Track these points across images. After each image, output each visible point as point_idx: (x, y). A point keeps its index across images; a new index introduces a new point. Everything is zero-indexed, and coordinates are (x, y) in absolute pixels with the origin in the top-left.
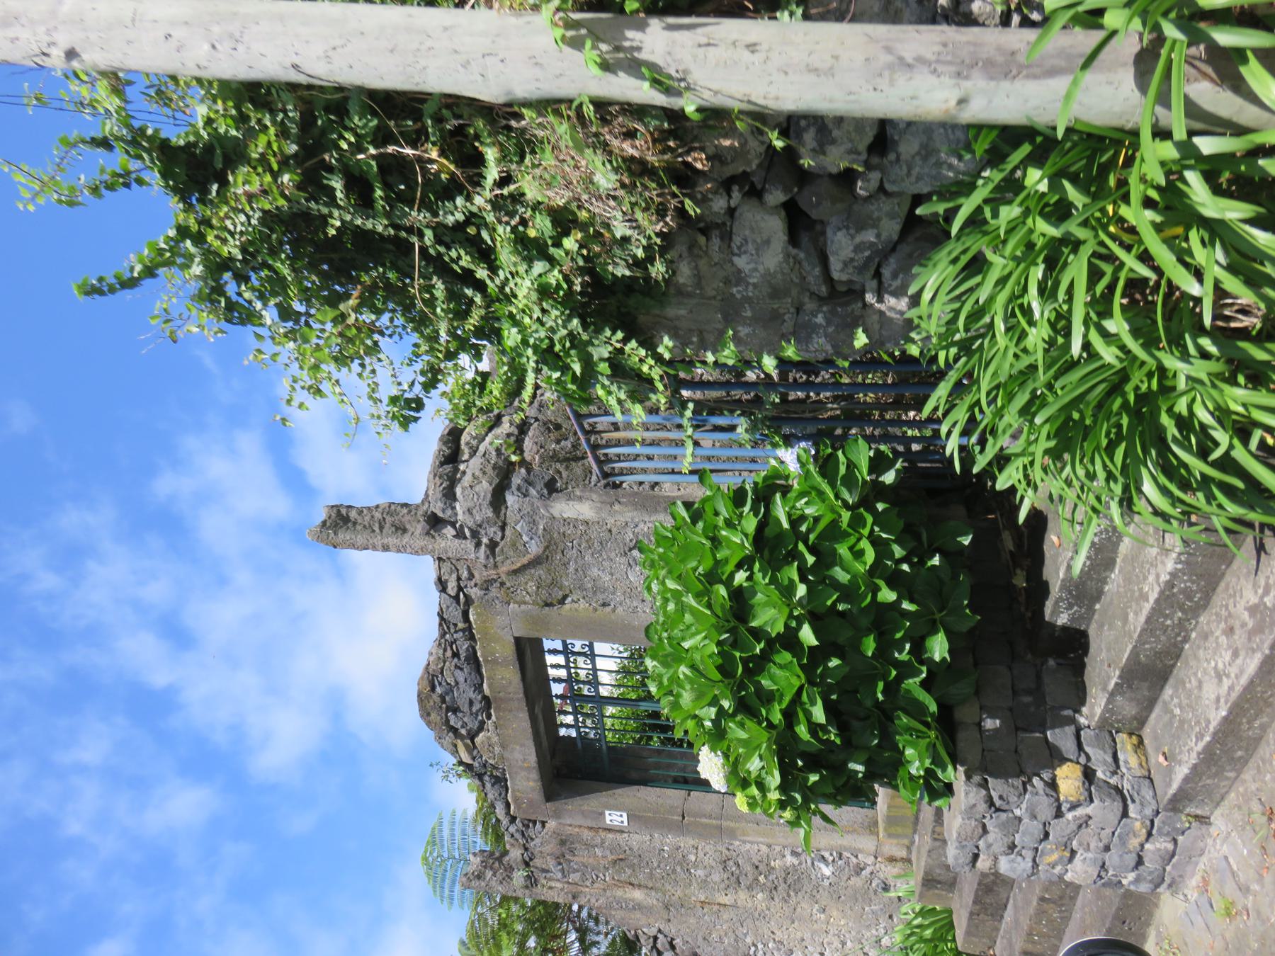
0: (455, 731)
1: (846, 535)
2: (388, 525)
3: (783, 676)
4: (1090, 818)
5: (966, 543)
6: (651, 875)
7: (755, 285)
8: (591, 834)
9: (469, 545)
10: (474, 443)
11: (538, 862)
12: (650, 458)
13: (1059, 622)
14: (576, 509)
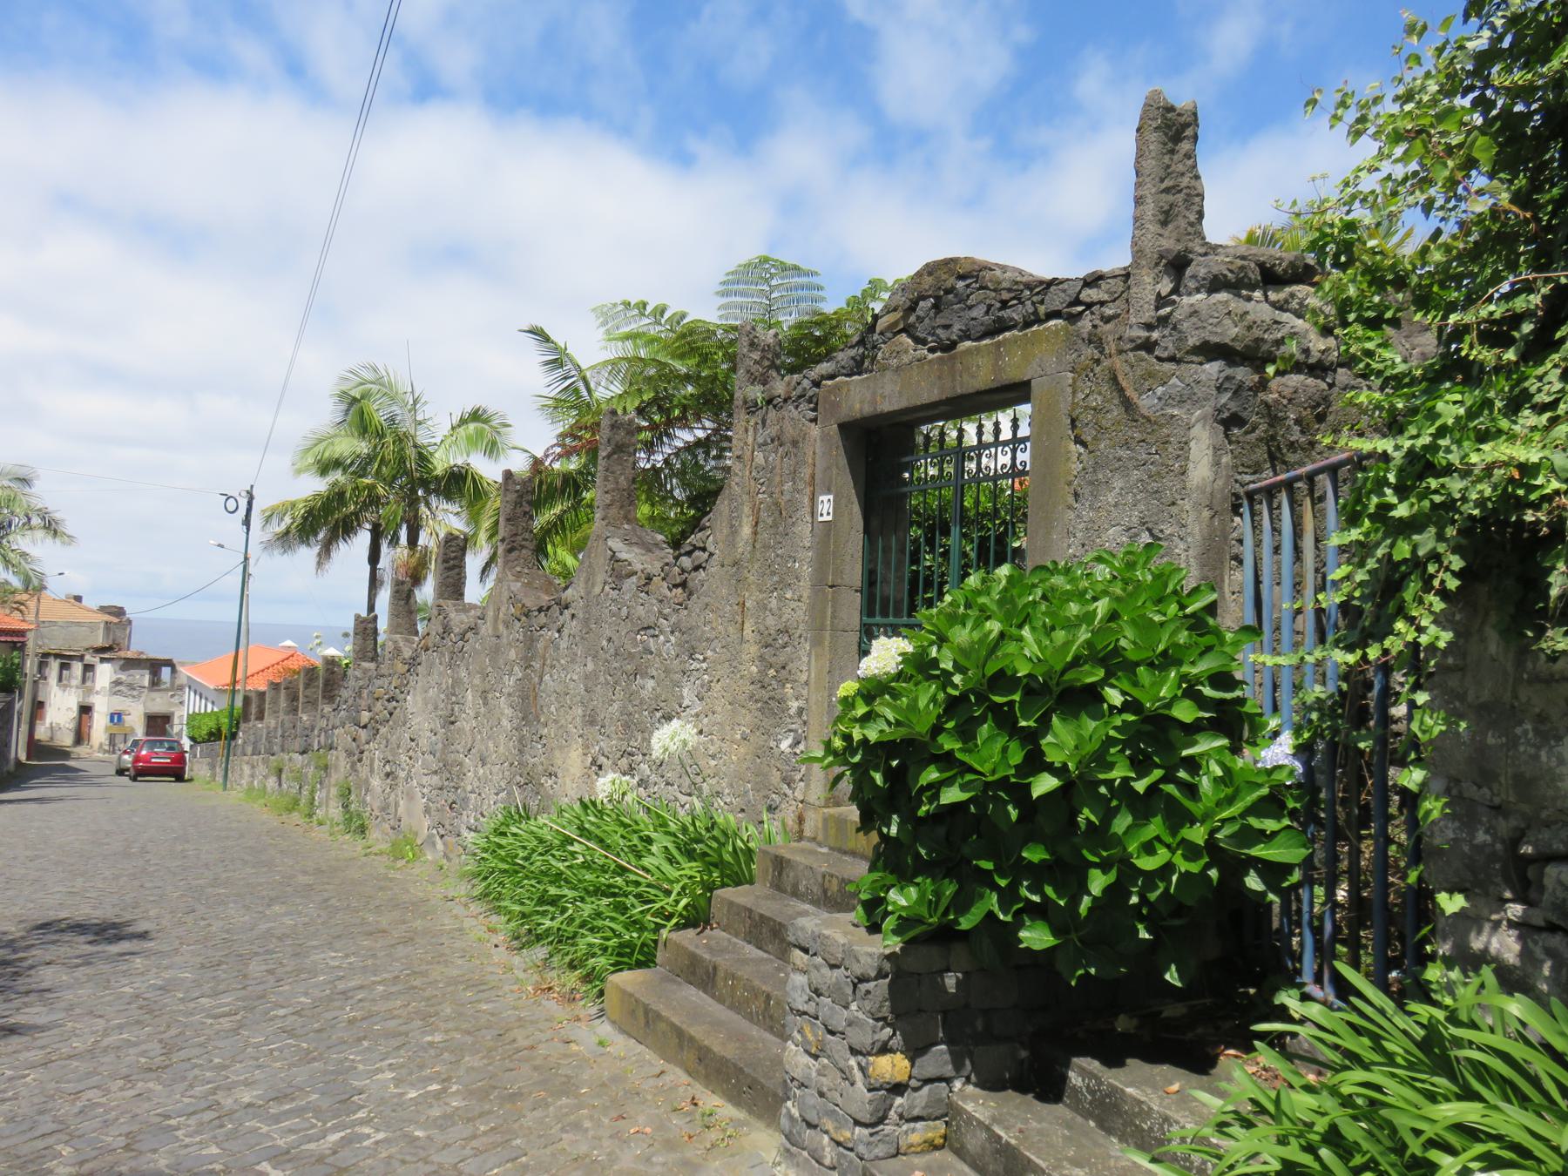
0: (912, 308)
1: (1174, 831)
2: (1170, 198)
3: (993, 754)
4: (852, 1084)
5: (1167, 977)
6: (766, 547)
7: (1536, 757)
8: (807, 477)
9: (1149, 315)
10: (1294, 304)
11: (772, 414)
12: (1277, 550)
13: (1071, 1074)
14: (1203, 460)
